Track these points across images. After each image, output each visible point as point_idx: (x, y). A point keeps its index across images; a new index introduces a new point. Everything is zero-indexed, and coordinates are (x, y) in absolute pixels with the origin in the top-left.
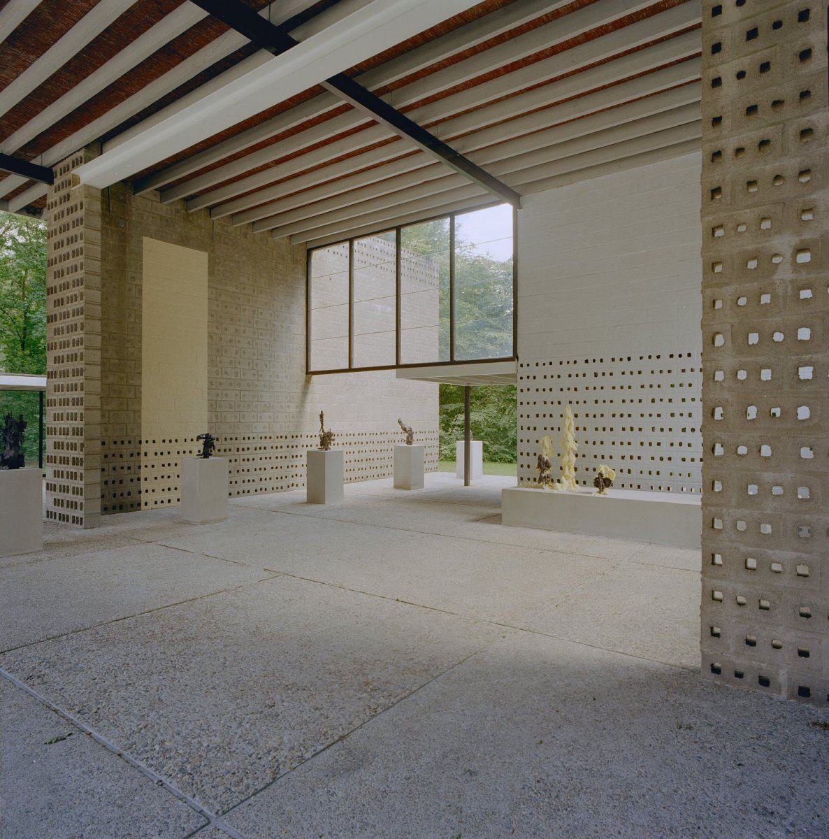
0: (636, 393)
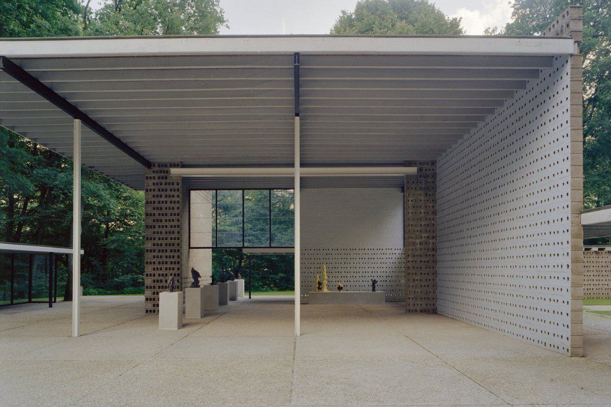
0: (340, 261)
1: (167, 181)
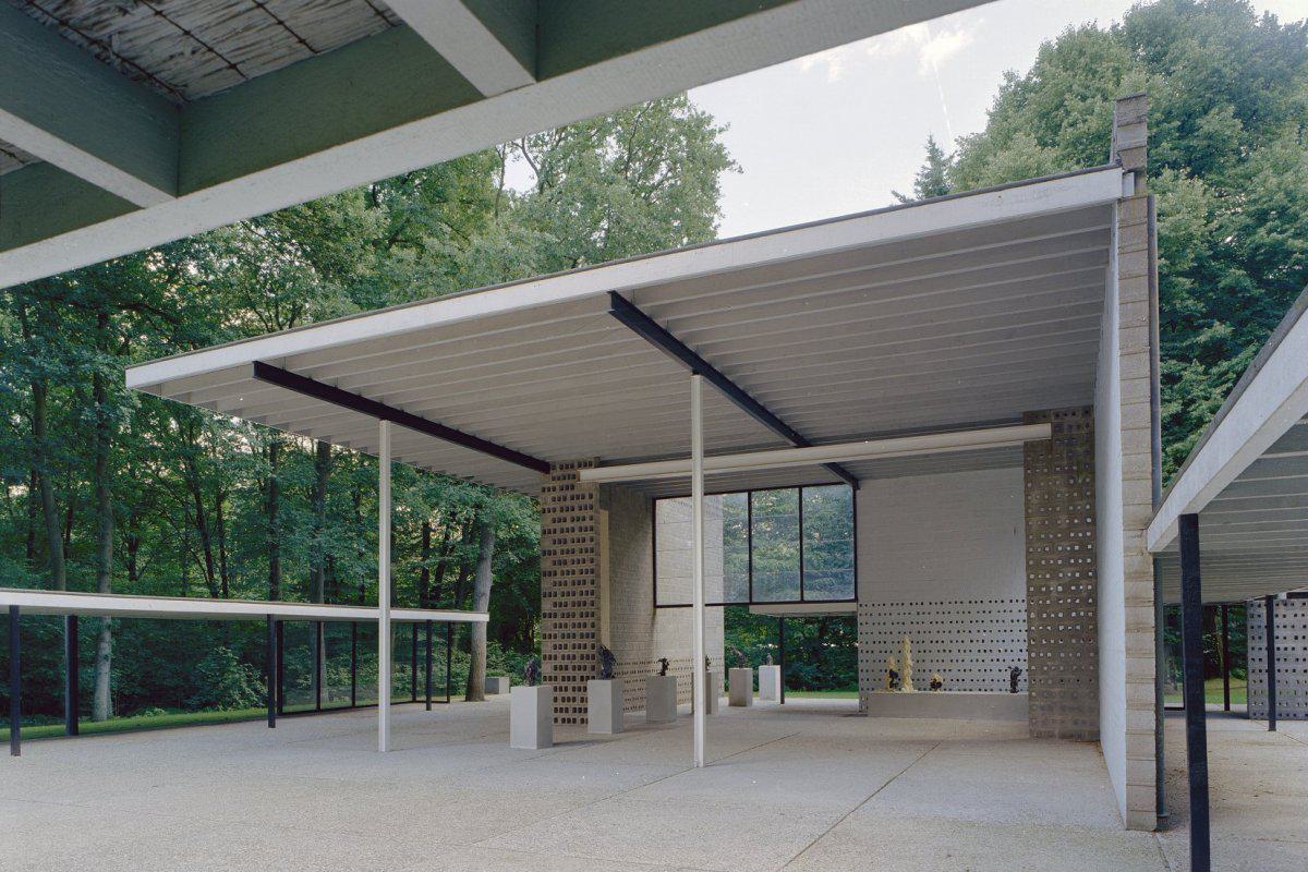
0: (947, 626)
1: (576, 492)
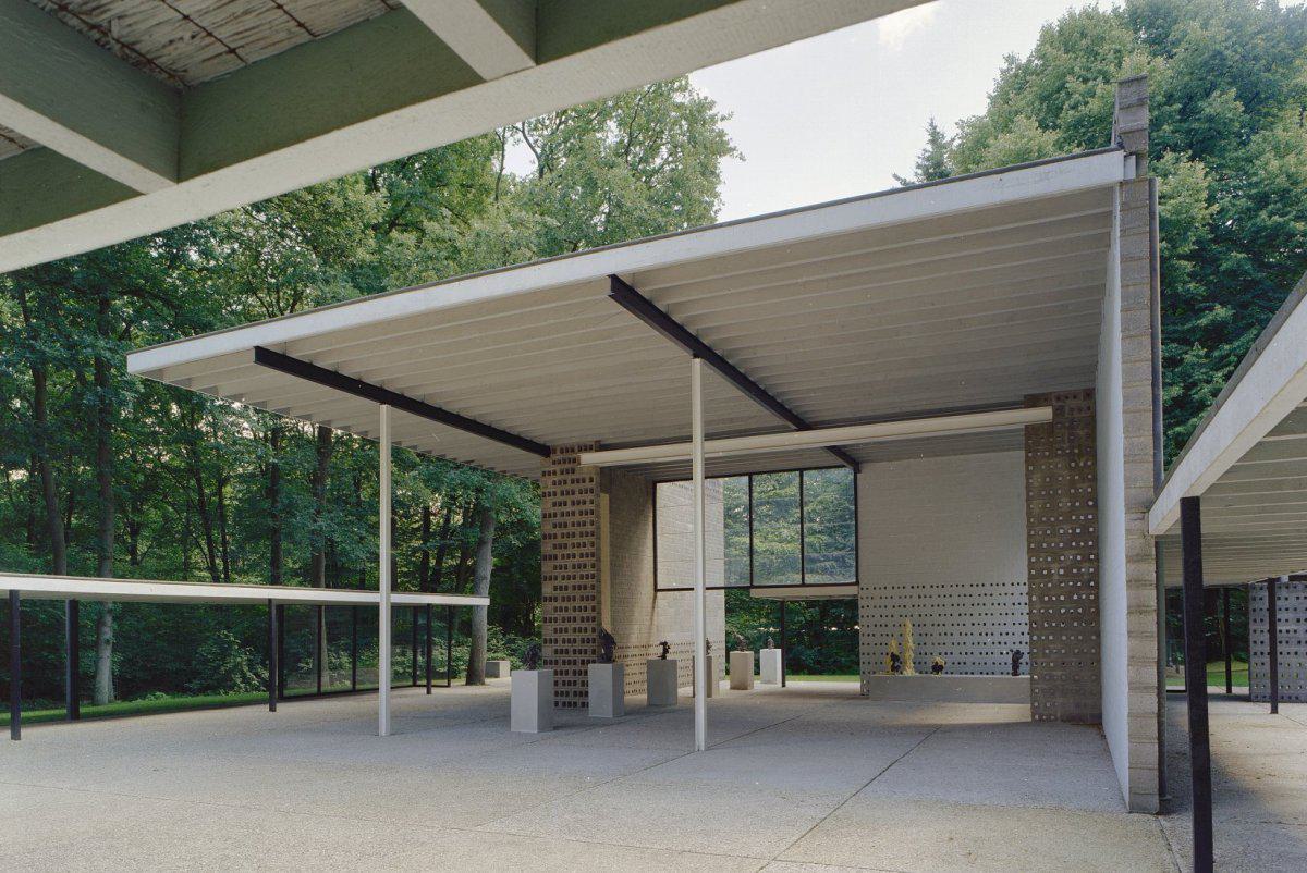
0: (949, 610)
